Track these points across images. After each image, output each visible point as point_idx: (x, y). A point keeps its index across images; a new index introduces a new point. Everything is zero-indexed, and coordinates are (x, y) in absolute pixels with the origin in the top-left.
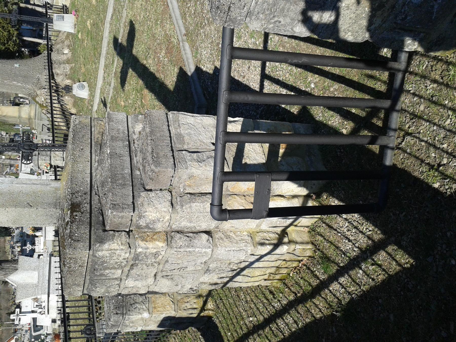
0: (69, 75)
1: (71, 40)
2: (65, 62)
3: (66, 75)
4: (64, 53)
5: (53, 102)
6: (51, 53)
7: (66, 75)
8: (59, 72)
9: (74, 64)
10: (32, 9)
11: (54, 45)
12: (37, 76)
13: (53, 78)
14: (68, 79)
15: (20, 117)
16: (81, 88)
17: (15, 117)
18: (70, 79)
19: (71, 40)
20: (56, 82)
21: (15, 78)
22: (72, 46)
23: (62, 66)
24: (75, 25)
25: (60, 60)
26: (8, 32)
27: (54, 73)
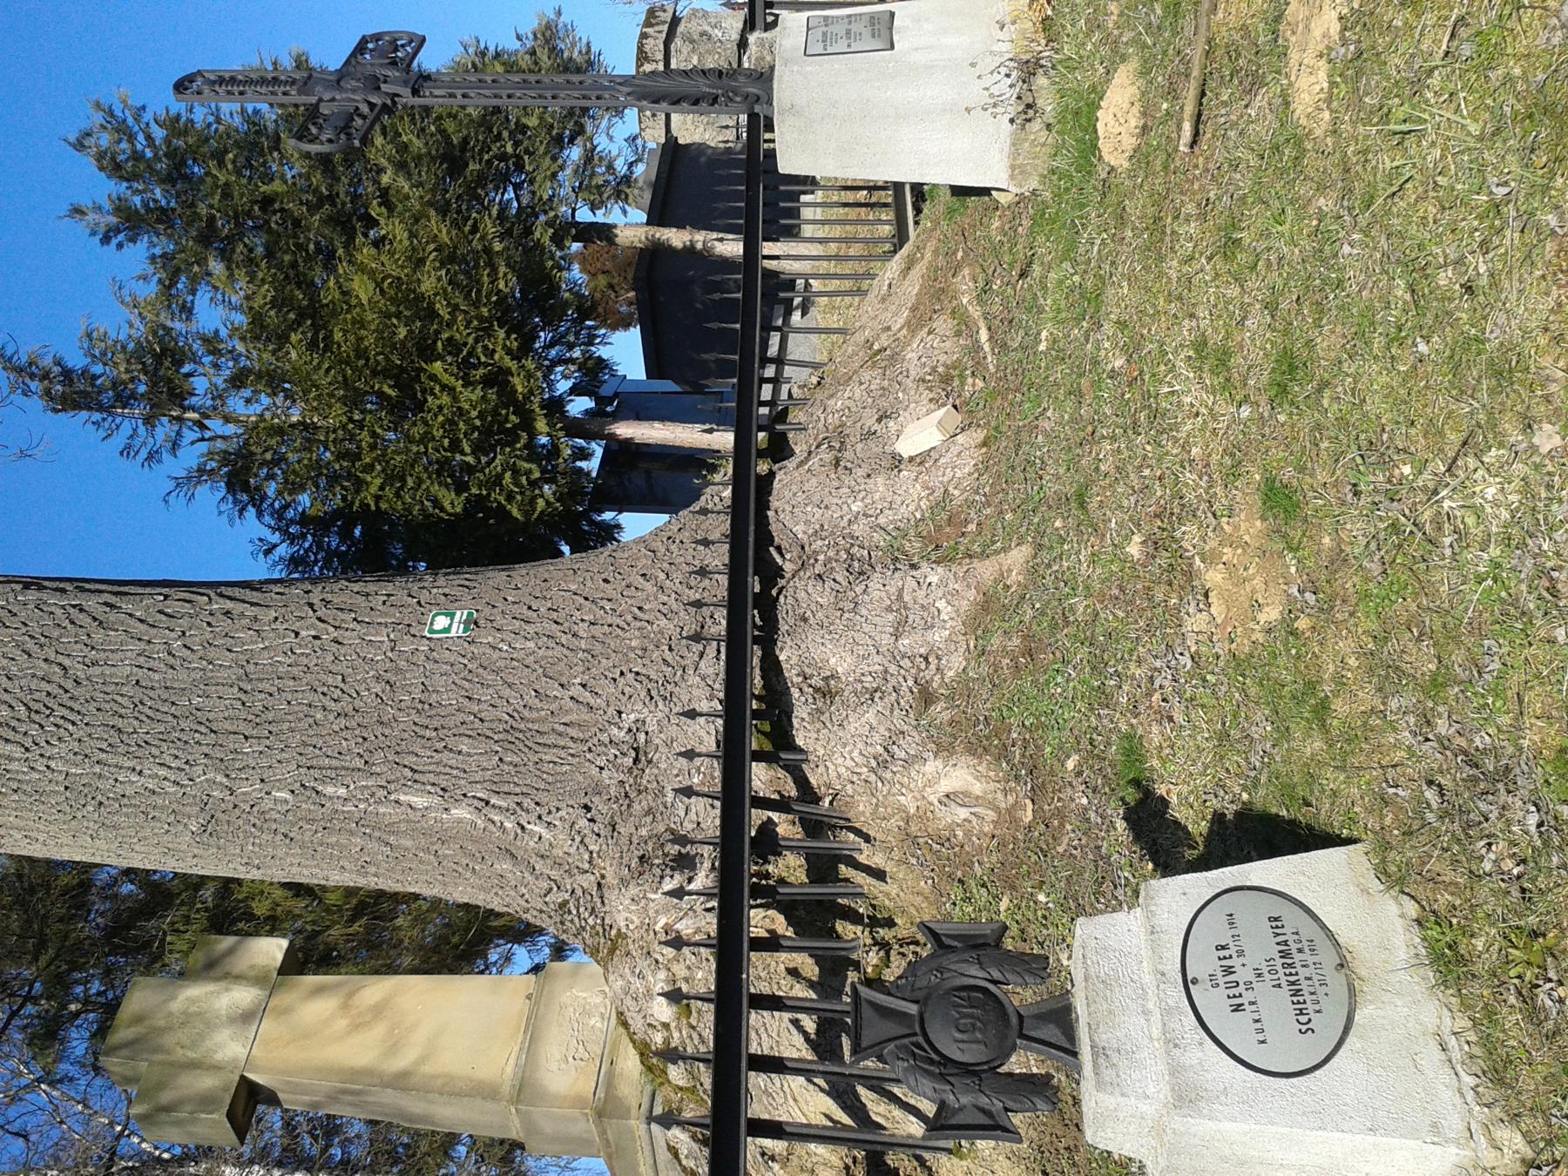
0: (962, 690)
1: (975, 312)
2: (913, 546)
3: (926, 697)
4: (897, 462)
5: (757, 1109)
6: (766, 482)
7: (926, 697)
8: (840, 662)
9: (1018, 557)
10: (690, 250)
11: (803, 401)
12: (629, 719)
13: (781, 746)
14: (944, 749)
15: (525, 1090)
16: (1275, 1003)
17: (487, 1092)
18: (976, 749)
19: (975, 312)
20: (808, 793)
21: (424, 758)
22: (979, 368)
23: (879, 588)
24: (1029, 69)
25: (859, 529)
26: (487, 382)
27: (791, 674)
